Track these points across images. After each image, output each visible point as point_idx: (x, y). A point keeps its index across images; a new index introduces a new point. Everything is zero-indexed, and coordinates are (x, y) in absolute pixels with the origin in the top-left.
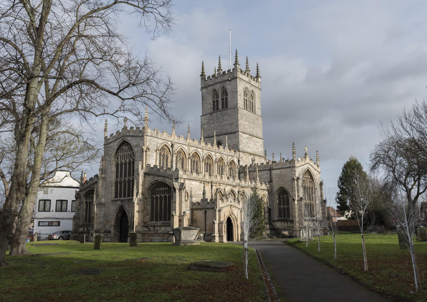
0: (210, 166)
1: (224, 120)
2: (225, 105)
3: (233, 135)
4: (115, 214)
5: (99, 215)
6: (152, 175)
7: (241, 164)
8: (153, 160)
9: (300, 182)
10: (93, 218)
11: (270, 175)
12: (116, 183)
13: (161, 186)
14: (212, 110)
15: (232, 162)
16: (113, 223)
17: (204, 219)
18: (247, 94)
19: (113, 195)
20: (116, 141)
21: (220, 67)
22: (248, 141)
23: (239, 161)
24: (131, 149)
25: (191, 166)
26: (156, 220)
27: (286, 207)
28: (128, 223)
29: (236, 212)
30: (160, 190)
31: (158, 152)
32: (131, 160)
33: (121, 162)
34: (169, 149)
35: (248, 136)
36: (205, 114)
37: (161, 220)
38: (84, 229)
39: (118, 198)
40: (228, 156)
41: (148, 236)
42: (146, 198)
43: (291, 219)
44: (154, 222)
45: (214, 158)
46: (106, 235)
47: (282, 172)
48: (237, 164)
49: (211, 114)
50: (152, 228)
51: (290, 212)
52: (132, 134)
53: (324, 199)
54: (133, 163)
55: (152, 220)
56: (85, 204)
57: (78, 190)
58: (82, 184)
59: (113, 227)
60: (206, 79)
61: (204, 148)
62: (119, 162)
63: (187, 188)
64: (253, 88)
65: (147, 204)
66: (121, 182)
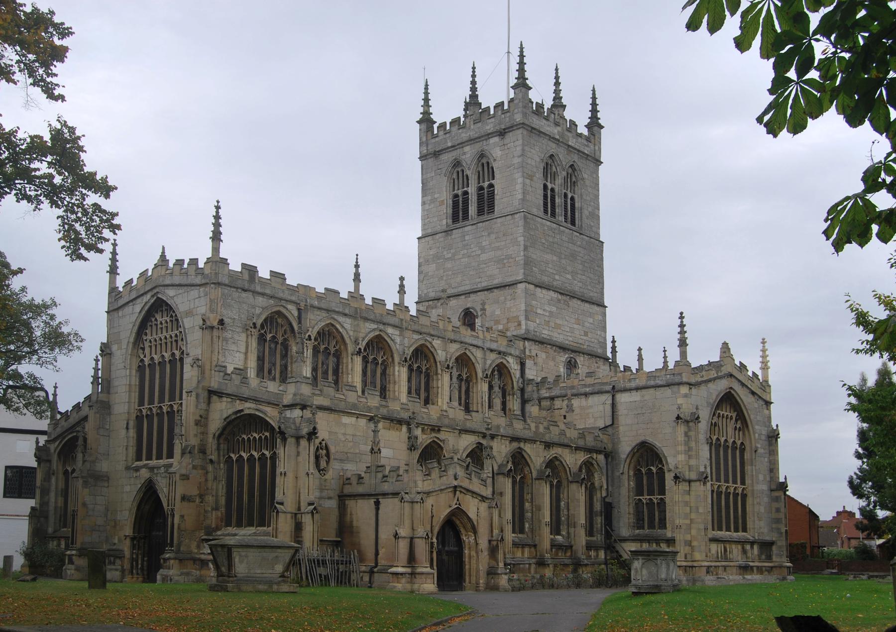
0: (428, 376)
1: (483, 250)
2: (487, 202)
3: (508, 291)
4: (135, 504)
5: (90, 507)
6: (228, 395)
8: (237, 355)
11: (613, 405)
12: (139, 419)
14: (450, 221)
15: (501, 370)
16: (128, 531)
18: (554, 176)
19: (132, 451)
20: (139, 300)
21: (474, 96)
22: (554, 309)
23: (523, 365)
24: (176, 322)
26: (239, 525)
27: (655, 498)
29: (472, 507)
32: (177, 353)
33: (152, 359)
36: (429, 231)
37: (250, 524)
38: (59, 545)
42: (211, 461)
43: (669, 535)
44: (230, 530)
45: (441, 355)
47: (646, 398)
48: (518, 374)
49: (448, 232)
52: (177, 280)
53: (782, 480)
54: (181, 360)
56: (61, 476)
57: (43, 439)
58: (54, 423)
59: (128, 542)
60: (436, 132)
62: (147, 361)
63: (322, 434)
64: (576, 158)
65: (215, 478)
66: (150, 417)
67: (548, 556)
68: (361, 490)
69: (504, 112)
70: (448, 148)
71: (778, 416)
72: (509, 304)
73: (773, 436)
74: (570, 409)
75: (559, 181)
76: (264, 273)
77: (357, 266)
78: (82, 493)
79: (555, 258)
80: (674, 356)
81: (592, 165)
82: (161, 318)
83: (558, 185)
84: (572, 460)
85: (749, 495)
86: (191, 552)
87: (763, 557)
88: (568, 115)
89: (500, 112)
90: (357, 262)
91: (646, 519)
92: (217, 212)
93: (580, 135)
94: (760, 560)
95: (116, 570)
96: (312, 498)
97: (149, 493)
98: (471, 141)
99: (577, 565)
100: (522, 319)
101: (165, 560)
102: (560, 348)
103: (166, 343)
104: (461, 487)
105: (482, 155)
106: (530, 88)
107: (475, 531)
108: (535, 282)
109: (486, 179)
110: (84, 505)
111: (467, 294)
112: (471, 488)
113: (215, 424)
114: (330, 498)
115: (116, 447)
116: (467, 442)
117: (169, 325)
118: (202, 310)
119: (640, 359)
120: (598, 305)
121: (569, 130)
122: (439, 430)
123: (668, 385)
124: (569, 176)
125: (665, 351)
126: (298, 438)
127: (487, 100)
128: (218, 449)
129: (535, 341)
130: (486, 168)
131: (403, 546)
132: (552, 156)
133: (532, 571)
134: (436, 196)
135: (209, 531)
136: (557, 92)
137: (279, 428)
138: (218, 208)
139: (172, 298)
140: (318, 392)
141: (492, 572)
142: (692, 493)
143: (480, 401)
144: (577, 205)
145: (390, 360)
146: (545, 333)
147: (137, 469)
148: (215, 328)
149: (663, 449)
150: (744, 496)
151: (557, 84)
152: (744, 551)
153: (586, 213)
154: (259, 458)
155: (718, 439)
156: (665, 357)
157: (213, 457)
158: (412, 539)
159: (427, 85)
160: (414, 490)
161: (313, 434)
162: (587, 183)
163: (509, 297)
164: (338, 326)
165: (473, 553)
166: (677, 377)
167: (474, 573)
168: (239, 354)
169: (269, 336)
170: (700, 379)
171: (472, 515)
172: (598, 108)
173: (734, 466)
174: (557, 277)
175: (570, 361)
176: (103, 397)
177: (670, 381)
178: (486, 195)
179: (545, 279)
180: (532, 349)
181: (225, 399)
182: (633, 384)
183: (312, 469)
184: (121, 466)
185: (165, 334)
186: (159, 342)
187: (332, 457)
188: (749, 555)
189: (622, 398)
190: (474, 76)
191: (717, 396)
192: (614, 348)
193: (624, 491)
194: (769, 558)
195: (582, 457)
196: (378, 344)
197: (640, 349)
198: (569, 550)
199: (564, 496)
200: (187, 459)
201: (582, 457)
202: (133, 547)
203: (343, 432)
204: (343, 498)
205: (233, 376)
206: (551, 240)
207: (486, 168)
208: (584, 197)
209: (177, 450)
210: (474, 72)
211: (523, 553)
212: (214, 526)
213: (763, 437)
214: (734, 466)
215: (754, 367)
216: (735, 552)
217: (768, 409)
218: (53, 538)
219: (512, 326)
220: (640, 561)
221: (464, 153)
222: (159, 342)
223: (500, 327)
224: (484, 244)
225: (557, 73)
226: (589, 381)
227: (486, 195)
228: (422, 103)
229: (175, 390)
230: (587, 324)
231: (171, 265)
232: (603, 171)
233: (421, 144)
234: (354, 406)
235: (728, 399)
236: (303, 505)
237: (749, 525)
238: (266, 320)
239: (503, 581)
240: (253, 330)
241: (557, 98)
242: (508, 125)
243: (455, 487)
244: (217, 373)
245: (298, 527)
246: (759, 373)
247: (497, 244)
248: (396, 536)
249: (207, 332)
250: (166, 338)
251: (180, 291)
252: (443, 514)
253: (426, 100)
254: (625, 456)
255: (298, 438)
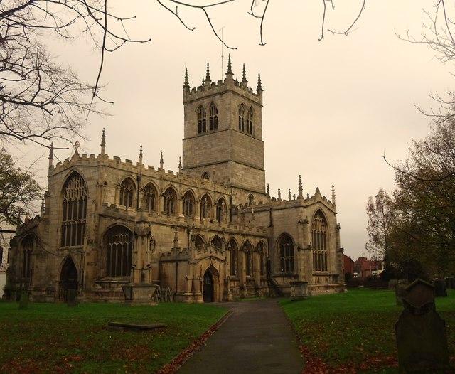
0: (191, 205)
2: (214, 124)
3: (224, 165)
6: (109, 217)
9: (309, 225)
10: (32, 271)
12: (63, 227)
16: (58, 279)
18: (243, 112)
19: (59, 242)
21: (208, 77)
23: (231, 200)
24: (83, 182)
25: (164, 205)
27: (289, 257)
28: (77, 278)
29: (217, 265)
31: (119, 187)
35: (244, 166)
37: (118, 275)
38: (21, 286)
45: (197, 195)
48: (229, 203)
49: (196, 137)
50: (107, 285)
51: (295, 265)
54: (86, 200)
55: (108, 275)
56: (22, 253)
57: (14, 235)
62: (68, 200)
63: (153, 234)
69: (222, 84)
71: (340, 219)
73: (338, 228)
74: (253, 218)
75: (245, 115)
76: (123, 161)
77: (162, 156)
78: (36, 262)
83: (245, 116)
84: (254, 242)
88: (249, 85)
93: (254, 94)
99: (257, 288)
101: (79, 292)
105: (212, 103)
110: (37, 267)
111: (205, 166)
113: (102, 230)
114: (155, 262)
115: (52, 237)
126: (143, 236)
128: (103, 241)
131: (189, 283)
138: (104, 131)
141: (226, 293)
144: (253, 125)
146: (240, 184)
147: (62, 250)
148: (102, 185)
150: (326, 255)
152: (327, 280)
161: (149, 234)
165: (218, 285)
166: (297, 204)
176: (46, 217)
180: (235, 191)
182: (279, 207)
184: (54, 249)
190: (208, 68)
192: (268, 189)
193: (276, 255)
195: (258, 240)
196: (171, 191)
197: (279, 189)
200: (90, 246)
203: (160, 232)
204: (161, 262)
207: (214, 109)
209: (86, 242)
215: (329, 198)
218: (18, 283)
229: (82, 212)
231: (81, 156)
233: (184, 97)
234: (166, 221)
235: (319, 213)
236: (145, 266)
239: (230, 297)
241: (244, 78)
243: (210, 257)
245: (143, 276)
248: (187, 279)
255: (143, 236)
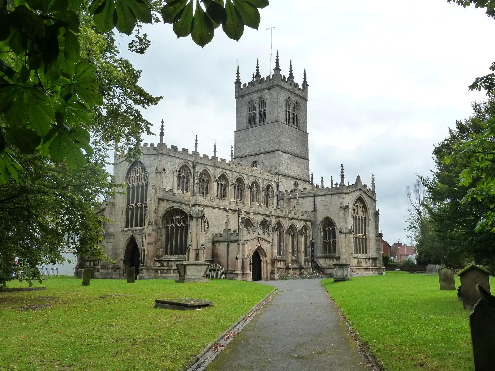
0: (241, 191)
1: (261, 137)
2: (263, 118)
3: (272, 154)
4: (126, 246)
5: (106, 247)
6: (167, 200)
7: (280, 189)
12: (127, 210)
13: (177, 213)
14: (248, 125)
16: (122, 257)
17: (227, 254)
18: (290, 106)
19: (124, 224)
21: (258, 73)
22: (289, 162)
24: (144, 169)
26: (171, 254)
27: (332, 240)
29: (265, 246)
30: (181, 218)
31: (177, 174)
33: (133, 185)
34: (190, 170)
36: (239, 129)
37: (176, 254)
38: (90, 264)
39: (130, 228)
40: (264, 179)
41: (161, 273)
42: (160, 228)
43: (337, 256)
44: (167, 256)
46: (114, 271)
53: (380, 232)
54: (146, 185)
55: (166, 253)
60: (242, 87)
61: (233, 170)
62: (131, 185)
64: (298, 98)
65: (161, 235)
67: (290, 265)
68: (221, 239)
69: (270, 80)
70: (247, 94)
72: (272, 160)
73: (377, 214)
76: (180, 149)
79: (290, 140)
80: (339, 181)
81: (304, 101)
82: (137, 168)
84: (299, 225)
85: (368, 239)
86: (150, 266)
87: (373, 264)
88: (295, 81)
89: (268, 80)
90: (215, 144)
91: (328, 249)
92: (162, 124)
93: (300, 89)
94: (372, 266)
95: (117, 274)
96: (202, 243)
97: (132, 242)
98: (257, 91)
99: (301, 268)
100: (277, 166)
101: (141, 270)
102: (292, 178)
103: (139, 178)
104: (261, 238)
105: (261, 98)
106: (281, 70)
107: (266, 256)
108: (282, 150)
109: (263, 107)
111: (255, 155)
112: (264, 238)
113: (161, 212)
114: (209, 243)
116: (260, 219)
117: (141, 170)
118: (156, 165)
119: (322, 182)
120: (306, 159)
121: (296, 87)
122: (249, 214)
123: (337, 194)
124: (295, 106)
125: (332, 178)
126: (197, 218)
127: (264, 74)
128: (163, 223)
129: (283, 175)
130: (263, 103)
131: (239, 262)
132: (289, 98)
133: (284, 271)
134: (242, 114)
135: (158, 257)
136: (291, 71)
137: (190, 214)
138: (162, 122)
139: (143, 159)
140: (204, 199)
141: (272, 273)
142: (346, 238)
143: (261, 201)
145: (227, 184)
146: (286, 172)
147: (126, 231)
148: (161, 172)
149: (335, 220)
150: (366, 239)
151: (291, 68)
152: (366, 262)
153: (302, 121)
154: (180, 226)
155: (356, 216)
156: (332, 181)
157: (160, 226)
158: (243, 259)
159: (238, 68)
160: (243, 240)
161: (203, 217)
162: (302, 108)
163: (272, 157)
164: (208, 170)
165: (265, 265)
166: (339, 190)
167: (265, 273)
168: (170, 182)
169: (181, 175)
170: (349, 191)
171: (265, 249)
172: (307, 78)
173: (362, 227)
174: (291, 148)
175: (295, 183)
177: (338, 192)
178: (262, 114)
179: (286, 149)
181: (166, 202)
182: (322, 193)
183: (203, 231)
185: (139, 174)
186: (136, 178)
187: (210, 226)
188: (368, 263)
189: (318, 199)
190: (258, 64)
191: (356, 198)
194: (375, 265)
195: (303, 223)
197: (322, 178)
198: (298, 263)
199: (296, 240)
201: (303, 223)
202: (125, 264)
204: (214, 243)
205: (169, 192)
206: (289, 133)
207: (263, 103)
208: (301, 115)
210: (258, 63)
211: (280, 264)
212: (160, 255)
213: (373, 215)
214: (362, 227)
216: (363, 262)
217: (375, 203)
218: (87, 261)
219: (273, 169)
220: (337, 268)
221: (254, 97)
222: (136, 178)
223: (268, 169)
224: (262, 134)
225: (291, 63)
226: (305, 192)
227: (262, 114)
228: (236, 75)
229: (144, 197)
230: (302, 168)
232: (310, 105)
237: (368, 251)
238: (180, 169)
240: (176, 173)
241: (291, 74)
242: (272, 85)
243: (259, 238)
244: (162, 191)
246: (371, 188)
247: (267, 135)
248: (237, 258)
249: (158, 174)
250: (139, 176)
251: (146, 157)
252: (254, 249)
253: (238, 74)
254: (319, 223)
